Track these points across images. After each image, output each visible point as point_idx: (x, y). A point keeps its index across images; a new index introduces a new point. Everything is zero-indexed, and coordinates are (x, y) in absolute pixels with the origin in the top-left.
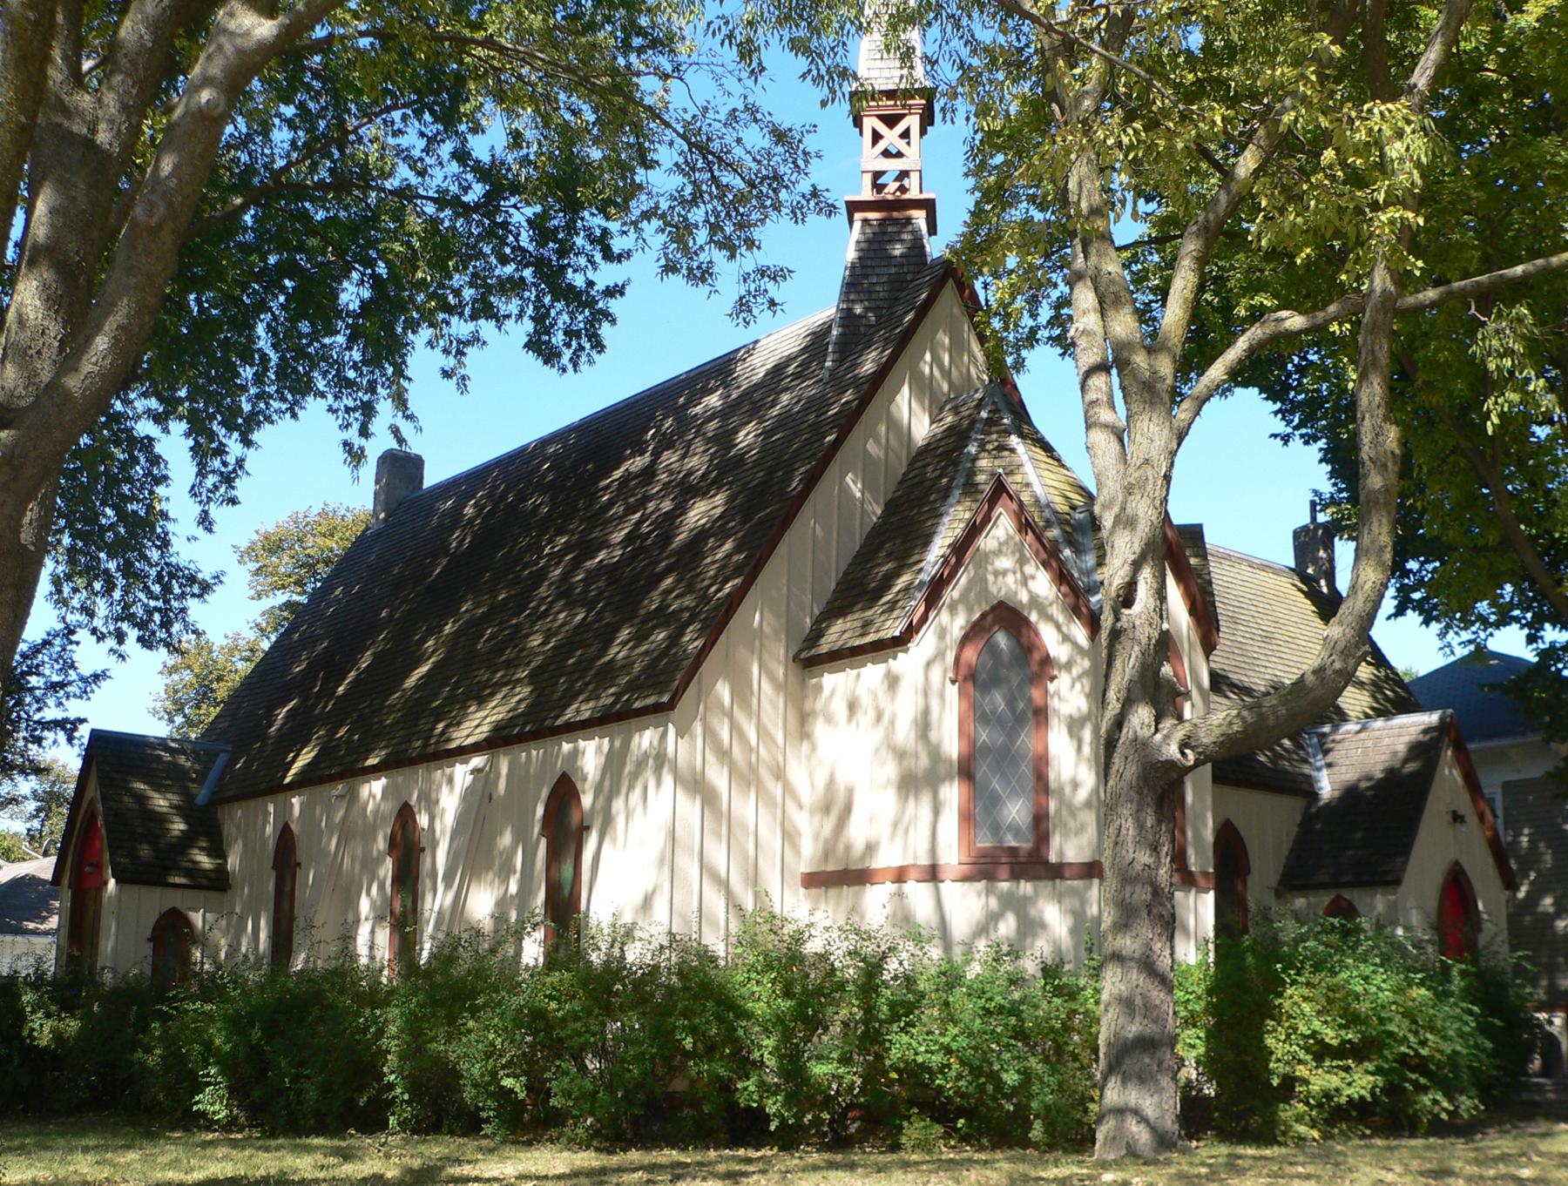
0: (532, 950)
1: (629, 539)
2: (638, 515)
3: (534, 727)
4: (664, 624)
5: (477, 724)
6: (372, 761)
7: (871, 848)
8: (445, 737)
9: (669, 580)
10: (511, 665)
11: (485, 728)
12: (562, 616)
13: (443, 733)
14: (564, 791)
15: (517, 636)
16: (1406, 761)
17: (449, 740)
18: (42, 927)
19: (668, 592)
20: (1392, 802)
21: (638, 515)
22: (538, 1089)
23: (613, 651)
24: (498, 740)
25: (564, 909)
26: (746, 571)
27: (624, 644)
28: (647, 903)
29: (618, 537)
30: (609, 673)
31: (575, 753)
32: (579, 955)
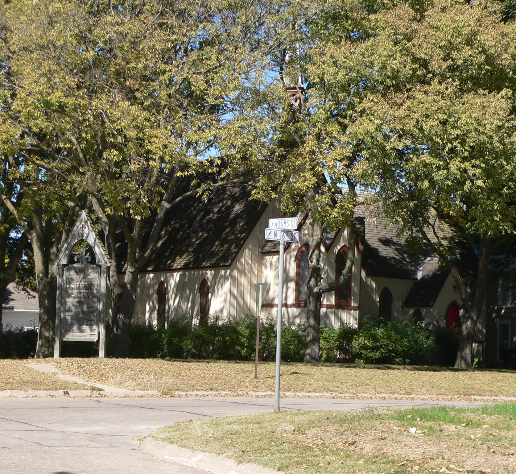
0: (195, 321)
1: (219, 212)
2: (221, 204)
3: (194, 265)
4: (227, 243)
5: (179, 262)
6: (150, 269)
7: (274, 299)
8: (171, 265)
9: (228, 229)
10: (188, 246)
11: (182, 264)
12: (201, 233)
13: (169, 264)
14: (204, 282)
15: (189, 237)
16: (438, 271)
17: (172, 266)
18: (7, 306)
19: (228, 233)
20: (436, 281)
21: (221, 204)
22: (200, 351)
23: (214, 248)
24: (185, 268)
25: (204, 311)
26: (247, 231)
27: (217, 246)
28: (222, 311)
29: (216, 210)
30: (213, 254)
31: (206, 273)
32: (206, 322)
